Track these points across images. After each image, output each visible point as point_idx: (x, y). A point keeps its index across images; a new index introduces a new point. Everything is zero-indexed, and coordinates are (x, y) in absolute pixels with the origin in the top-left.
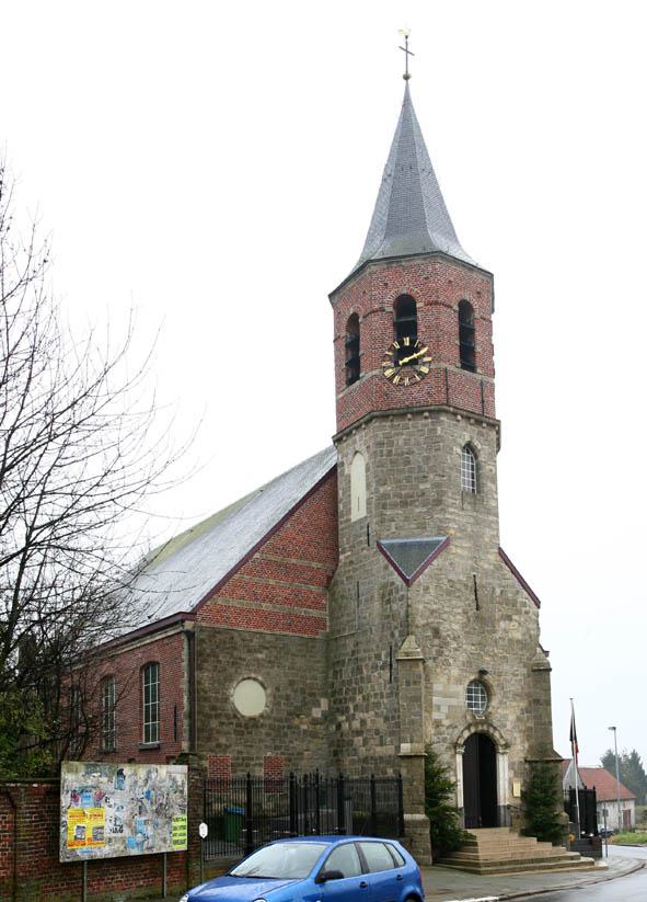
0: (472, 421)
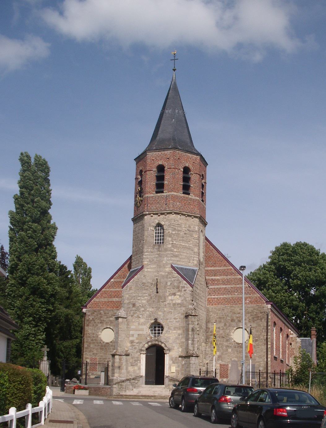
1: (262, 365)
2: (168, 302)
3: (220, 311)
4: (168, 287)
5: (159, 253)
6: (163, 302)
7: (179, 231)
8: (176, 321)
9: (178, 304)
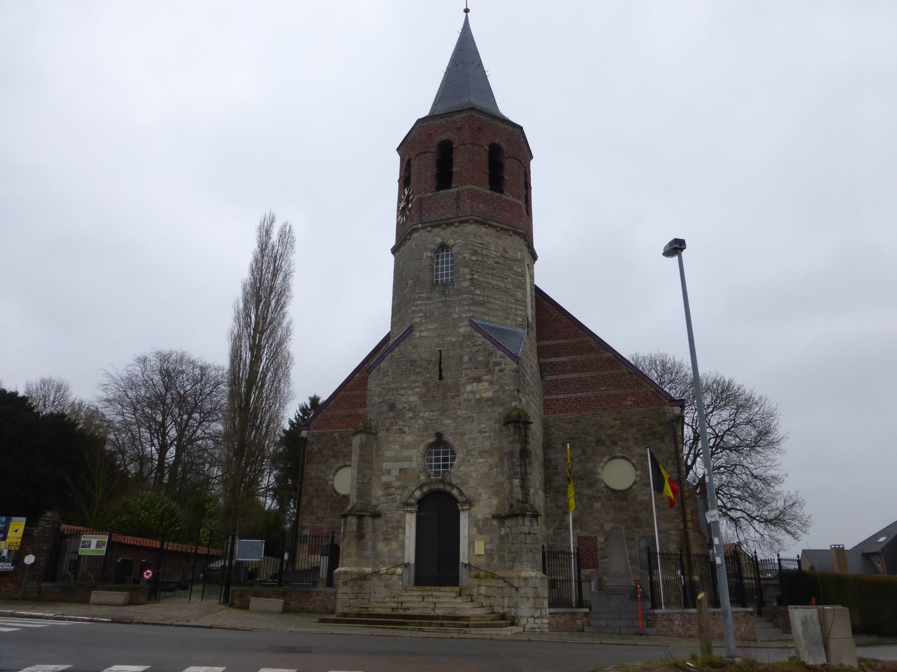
0: (499, 229)
1: (673, 538)
2: (465, 396)
3: (571, 425)
4: (464, 366)
5: (443, 299)
6: (453, 397)
7: (483, 255)
8: (483, 437)
9: (488, 400)
